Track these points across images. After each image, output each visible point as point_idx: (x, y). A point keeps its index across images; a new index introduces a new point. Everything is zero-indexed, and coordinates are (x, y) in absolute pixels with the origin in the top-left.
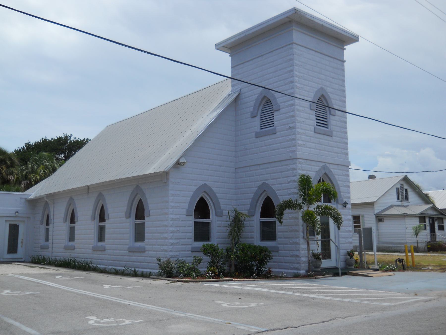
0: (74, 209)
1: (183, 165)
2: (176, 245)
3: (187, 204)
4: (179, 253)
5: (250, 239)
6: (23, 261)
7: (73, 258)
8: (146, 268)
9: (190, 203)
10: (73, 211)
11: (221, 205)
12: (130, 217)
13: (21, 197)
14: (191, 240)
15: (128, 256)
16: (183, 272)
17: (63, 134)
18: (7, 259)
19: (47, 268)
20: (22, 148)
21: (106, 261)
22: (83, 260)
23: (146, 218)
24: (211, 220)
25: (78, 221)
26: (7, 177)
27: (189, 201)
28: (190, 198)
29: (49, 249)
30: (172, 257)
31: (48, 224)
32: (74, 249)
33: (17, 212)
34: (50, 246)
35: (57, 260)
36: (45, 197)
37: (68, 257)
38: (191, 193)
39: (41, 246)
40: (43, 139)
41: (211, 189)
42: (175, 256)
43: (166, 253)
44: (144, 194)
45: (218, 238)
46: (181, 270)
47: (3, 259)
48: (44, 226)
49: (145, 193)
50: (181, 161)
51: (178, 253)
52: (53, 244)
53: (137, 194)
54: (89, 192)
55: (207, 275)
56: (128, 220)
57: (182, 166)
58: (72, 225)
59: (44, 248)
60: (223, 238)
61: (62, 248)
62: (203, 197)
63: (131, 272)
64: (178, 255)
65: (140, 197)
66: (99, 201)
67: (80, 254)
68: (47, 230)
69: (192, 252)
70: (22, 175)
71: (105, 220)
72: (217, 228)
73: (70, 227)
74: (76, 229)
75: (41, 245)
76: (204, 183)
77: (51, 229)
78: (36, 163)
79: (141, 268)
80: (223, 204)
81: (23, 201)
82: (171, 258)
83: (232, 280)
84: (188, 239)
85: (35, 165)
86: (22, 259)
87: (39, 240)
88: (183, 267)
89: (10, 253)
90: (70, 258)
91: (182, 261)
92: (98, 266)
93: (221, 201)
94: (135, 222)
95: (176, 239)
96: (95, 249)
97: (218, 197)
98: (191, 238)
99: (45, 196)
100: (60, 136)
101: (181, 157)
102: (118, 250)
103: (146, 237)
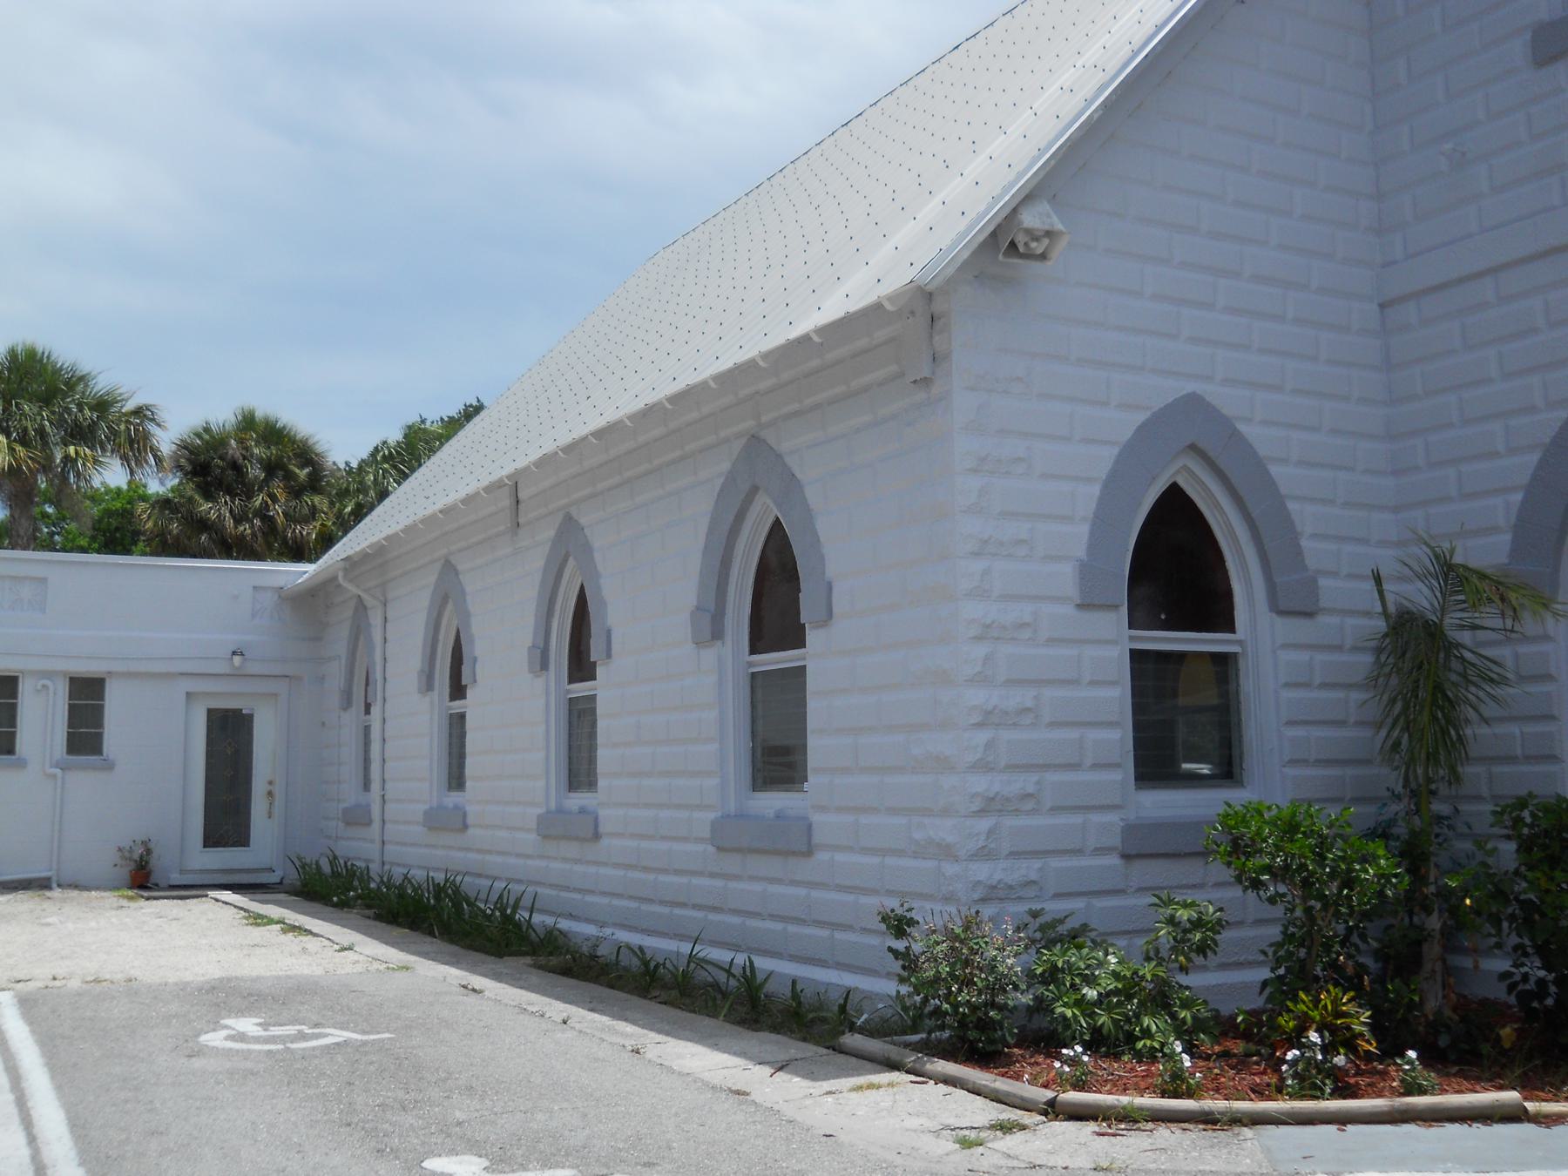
1: (1043, 257)
2: (1017, 812)
3: (1084, 530)
4: (1037, 864)
5: (1524, 768)
6: (278, 881)
8: (822, 963)
9: (1102, 521)
11: (1304, 543)
12: (717, 634)
14: (1117, 776)
15: (712, 875)
16: (1084, 1015)
18: (202, 871)
19: (309, 932)
22: (500, 885)
23: (811, 636)
24: (1240, 643)
25: (475, 681)
26: (294, 529)
27: (1093, 506)
28: (1096, 490)
30: (993, 893)
36: (340, 575)
38: (1108, 455)
39: (345, 811)
41: (1235, 435)
42: (1011, 887)
43: (950, 869)
44: (791, 486)
45: (1293, 762)
46: (1065, 1005)
47: (182, 872)
49: (798, 475)
50: (1031, 219)
51: (1028, 869)
52: (384, 801)
53: (754, 490)
55: (1290, 1056)
56: (709, 655)
57: (1036, 266)
58: (581, 689)
60: (1328, 762)
62: (1182, 483)
63: (730, 983)
64: (1034, 882)
65: (776, 512)
66: (565, 561)
67: (488, 858)
68: (457, 723)
69: (1127, 857)
71: (595, 663)
72: (1287, 694)
75: (346, 805)
76: (1184, 392)
78: (395, 467)
79: (794, 958)
80: (1314, 536)
82: (983, 900)
83: (1514, 1116)
84: (1096, 766)
85: (392, 476)
86: (274, 871)
88: (1077, 981)
91: (1062, 929)
92: (564, 924)
93: (1305, 516)
94: (750, 664)
95: (1013, 768)
96: (553, 827)
97: (1283, 490)
98: (1118, 766)
101: (1029, 197)
102: (664, 838)
103: (813, 759)
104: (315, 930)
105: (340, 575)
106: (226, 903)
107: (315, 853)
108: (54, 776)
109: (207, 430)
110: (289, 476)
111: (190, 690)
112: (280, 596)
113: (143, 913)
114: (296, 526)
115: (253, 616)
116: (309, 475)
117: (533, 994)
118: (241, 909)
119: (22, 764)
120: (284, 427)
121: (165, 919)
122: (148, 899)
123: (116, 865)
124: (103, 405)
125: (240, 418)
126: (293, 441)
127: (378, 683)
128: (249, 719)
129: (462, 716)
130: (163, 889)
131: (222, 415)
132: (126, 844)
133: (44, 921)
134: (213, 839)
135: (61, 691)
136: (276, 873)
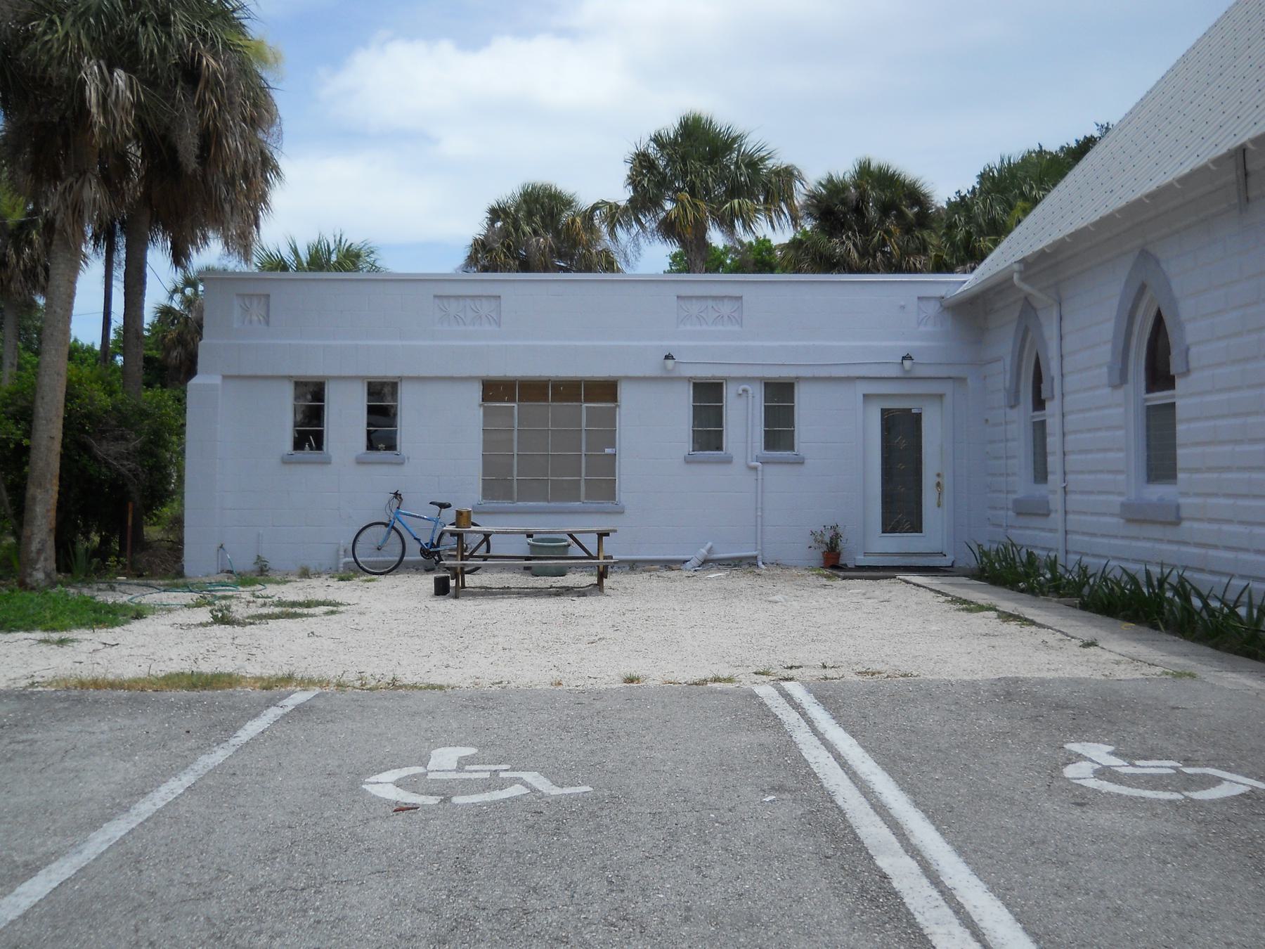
0: (1164, 314)
7: (1173, 567)
10: (1159, 321)
13: (922, 295)
17: (1098, 125)
20: (968, 192)
21: (1229, 555)
22: (1238, 583)
29: (1053, 515)
31: (1039, 403)
32: (1177, 522)
33: (910, 358)
34: (1056, 501)
35: (1090, 571)
36: (1016, 277)
37: (1146, 563)
39: (1016, 502)
40: (1033, 155)
47: (865, 554)
48: (1023, 413)
54: (1248, 199)
56: (1119, 394)
58: (1160, 397)
59: (1033, 510)
61: (1112, 515)
68: (1040, 429)
70: (953, 244)
73: (1148, 408)
74: (1180, 413)
75: (1014, 496)
77: (1053, 425)
81: (932, 308)
87: (1008, 475)
89: (893, 531)
90: (1156, 571)
94: (1146, 400)
99: (1016, 267)
100: (1088, 136)
104: (1038, 620)
105: (1016, 277)
106: (918, 586)
107: (990, 539)
108: (755, 469)
109: (830, 180)
110: (901, 215)
111: (866, 392)
112: (941, 306)
113: (852, 593)
114: (909, 258)
115: (919, 324)
116: (917, 214)
117: (56, 496)
118: (939, 592)
119: (728, 461)
120: (893, 175)
121: (876, 600)
122: (844, 578)
123: (810, 547)
124: (753, 164)
125: (857, 168)
126: (903, 184)
127: (1055, 380)
128: (918, 417)
129: (1043, 423)
130: (851, 570)
131: (844, 169)
132: (818, 528)
133: (770, 599)
134: (890, 526)
135: (757, 395)
136: (947, 557)
